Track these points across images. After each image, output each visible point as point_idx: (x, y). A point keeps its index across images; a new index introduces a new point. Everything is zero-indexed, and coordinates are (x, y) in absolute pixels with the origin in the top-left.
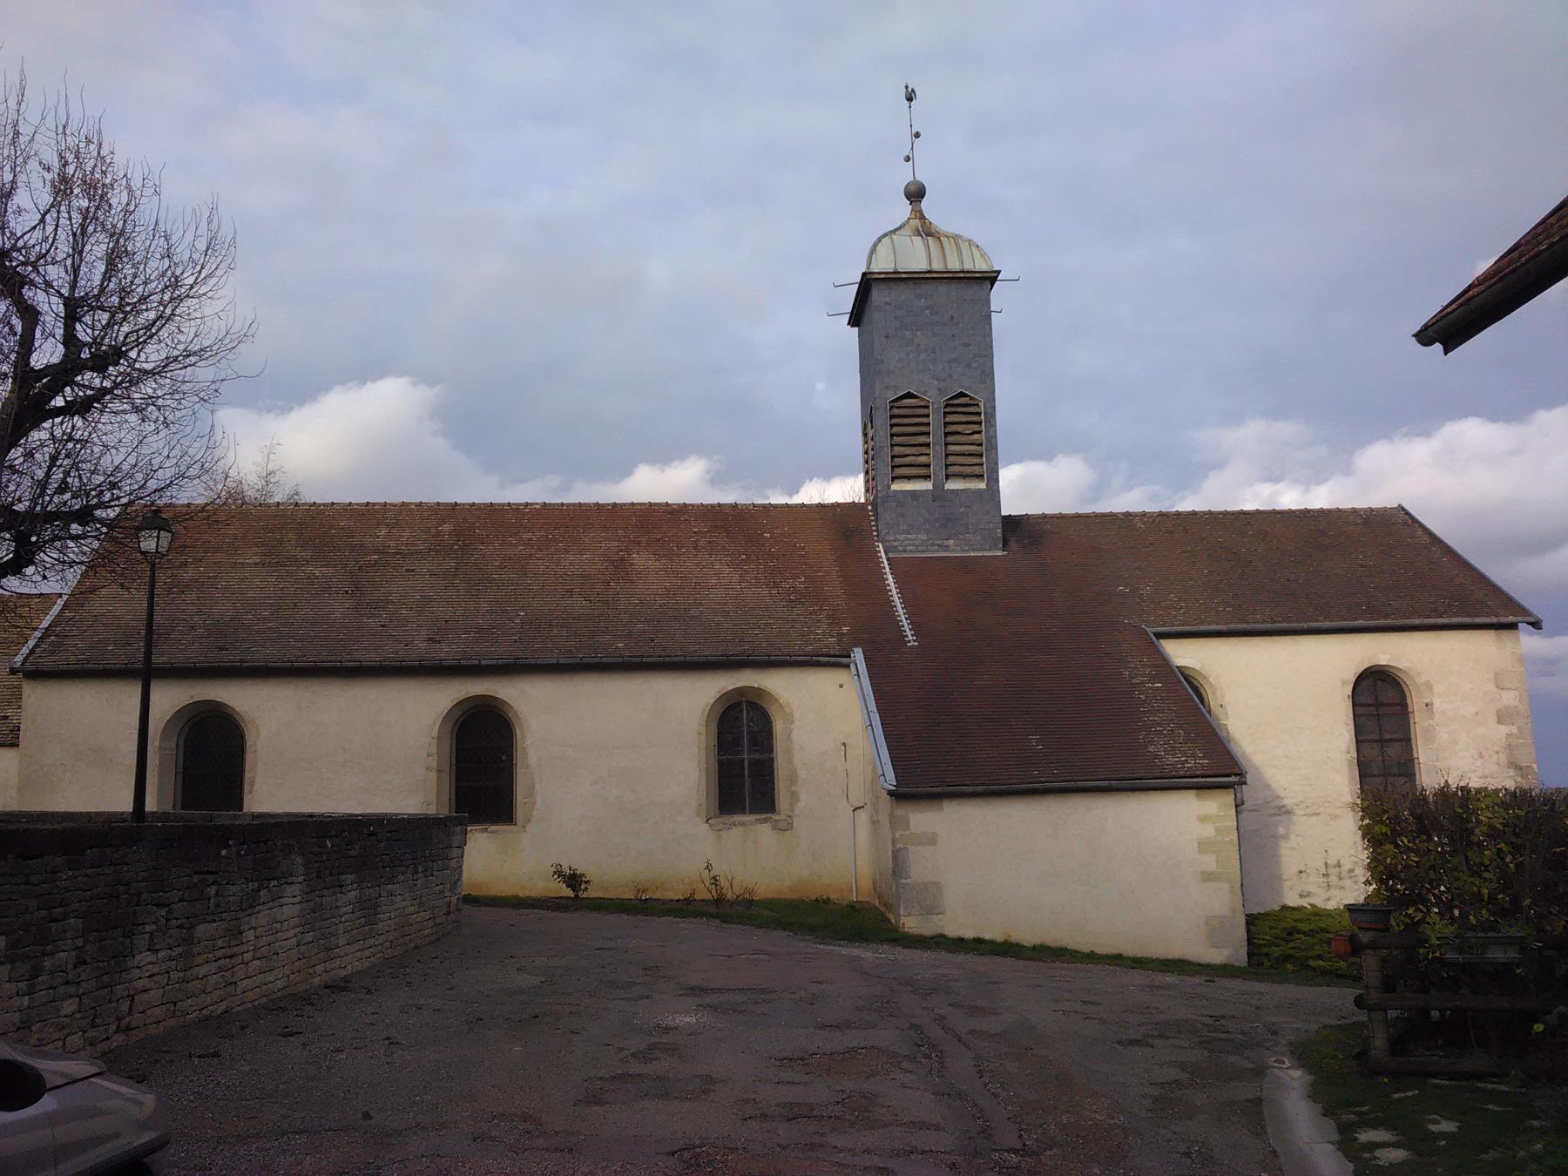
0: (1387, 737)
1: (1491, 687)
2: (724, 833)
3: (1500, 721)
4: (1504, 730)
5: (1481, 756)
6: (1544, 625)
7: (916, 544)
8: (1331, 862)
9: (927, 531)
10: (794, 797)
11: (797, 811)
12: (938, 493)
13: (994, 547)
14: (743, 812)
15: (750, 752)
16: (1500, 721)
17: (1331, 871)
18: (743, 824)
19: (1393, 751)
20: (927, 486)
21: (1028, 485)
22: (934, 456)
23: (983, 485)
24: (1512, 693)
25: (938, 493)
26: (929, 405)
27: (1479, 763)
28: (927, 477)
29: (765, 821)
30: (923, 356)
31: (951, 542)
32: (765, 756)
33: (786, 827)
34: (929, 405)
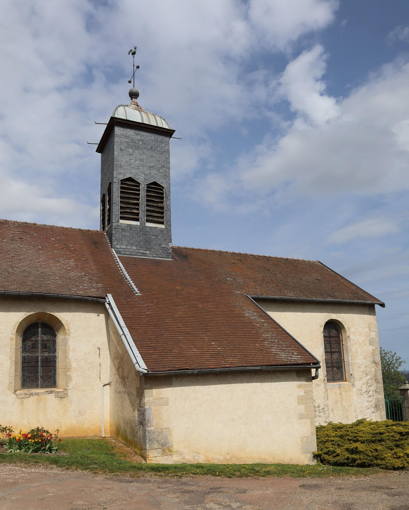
0: (333, 350)
1: (367, 330)
2: (25, 400)
3: (370, 344)
4: (371, 348)
5: (365, 358)
6: (386, 306)
7: (132, 249)
8: (316, 405)
9: (136, 246)
10: (69, 379)
11: (70, 387)
12: (143, 228)
13: (168, 257)
14: (37, 387)
15: (42, 352)
16: (370, 344)
17: (317, 409)
18: (37, 394)
19: (335, 356)
20: (138, 223)
21: (186, 232)
22: (142, 215)
23: (163, 226)
24: (374, 333)
25: (143, 228)
26: (137, 199)
27: (364, 361)
28: (137, 220)
29: (51, 392)
30: (137, 162)
31: (148, 252)
32: (51, 354)
33: (62, 396)
34: (137, 199)
